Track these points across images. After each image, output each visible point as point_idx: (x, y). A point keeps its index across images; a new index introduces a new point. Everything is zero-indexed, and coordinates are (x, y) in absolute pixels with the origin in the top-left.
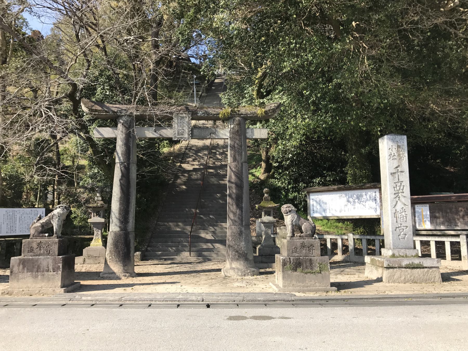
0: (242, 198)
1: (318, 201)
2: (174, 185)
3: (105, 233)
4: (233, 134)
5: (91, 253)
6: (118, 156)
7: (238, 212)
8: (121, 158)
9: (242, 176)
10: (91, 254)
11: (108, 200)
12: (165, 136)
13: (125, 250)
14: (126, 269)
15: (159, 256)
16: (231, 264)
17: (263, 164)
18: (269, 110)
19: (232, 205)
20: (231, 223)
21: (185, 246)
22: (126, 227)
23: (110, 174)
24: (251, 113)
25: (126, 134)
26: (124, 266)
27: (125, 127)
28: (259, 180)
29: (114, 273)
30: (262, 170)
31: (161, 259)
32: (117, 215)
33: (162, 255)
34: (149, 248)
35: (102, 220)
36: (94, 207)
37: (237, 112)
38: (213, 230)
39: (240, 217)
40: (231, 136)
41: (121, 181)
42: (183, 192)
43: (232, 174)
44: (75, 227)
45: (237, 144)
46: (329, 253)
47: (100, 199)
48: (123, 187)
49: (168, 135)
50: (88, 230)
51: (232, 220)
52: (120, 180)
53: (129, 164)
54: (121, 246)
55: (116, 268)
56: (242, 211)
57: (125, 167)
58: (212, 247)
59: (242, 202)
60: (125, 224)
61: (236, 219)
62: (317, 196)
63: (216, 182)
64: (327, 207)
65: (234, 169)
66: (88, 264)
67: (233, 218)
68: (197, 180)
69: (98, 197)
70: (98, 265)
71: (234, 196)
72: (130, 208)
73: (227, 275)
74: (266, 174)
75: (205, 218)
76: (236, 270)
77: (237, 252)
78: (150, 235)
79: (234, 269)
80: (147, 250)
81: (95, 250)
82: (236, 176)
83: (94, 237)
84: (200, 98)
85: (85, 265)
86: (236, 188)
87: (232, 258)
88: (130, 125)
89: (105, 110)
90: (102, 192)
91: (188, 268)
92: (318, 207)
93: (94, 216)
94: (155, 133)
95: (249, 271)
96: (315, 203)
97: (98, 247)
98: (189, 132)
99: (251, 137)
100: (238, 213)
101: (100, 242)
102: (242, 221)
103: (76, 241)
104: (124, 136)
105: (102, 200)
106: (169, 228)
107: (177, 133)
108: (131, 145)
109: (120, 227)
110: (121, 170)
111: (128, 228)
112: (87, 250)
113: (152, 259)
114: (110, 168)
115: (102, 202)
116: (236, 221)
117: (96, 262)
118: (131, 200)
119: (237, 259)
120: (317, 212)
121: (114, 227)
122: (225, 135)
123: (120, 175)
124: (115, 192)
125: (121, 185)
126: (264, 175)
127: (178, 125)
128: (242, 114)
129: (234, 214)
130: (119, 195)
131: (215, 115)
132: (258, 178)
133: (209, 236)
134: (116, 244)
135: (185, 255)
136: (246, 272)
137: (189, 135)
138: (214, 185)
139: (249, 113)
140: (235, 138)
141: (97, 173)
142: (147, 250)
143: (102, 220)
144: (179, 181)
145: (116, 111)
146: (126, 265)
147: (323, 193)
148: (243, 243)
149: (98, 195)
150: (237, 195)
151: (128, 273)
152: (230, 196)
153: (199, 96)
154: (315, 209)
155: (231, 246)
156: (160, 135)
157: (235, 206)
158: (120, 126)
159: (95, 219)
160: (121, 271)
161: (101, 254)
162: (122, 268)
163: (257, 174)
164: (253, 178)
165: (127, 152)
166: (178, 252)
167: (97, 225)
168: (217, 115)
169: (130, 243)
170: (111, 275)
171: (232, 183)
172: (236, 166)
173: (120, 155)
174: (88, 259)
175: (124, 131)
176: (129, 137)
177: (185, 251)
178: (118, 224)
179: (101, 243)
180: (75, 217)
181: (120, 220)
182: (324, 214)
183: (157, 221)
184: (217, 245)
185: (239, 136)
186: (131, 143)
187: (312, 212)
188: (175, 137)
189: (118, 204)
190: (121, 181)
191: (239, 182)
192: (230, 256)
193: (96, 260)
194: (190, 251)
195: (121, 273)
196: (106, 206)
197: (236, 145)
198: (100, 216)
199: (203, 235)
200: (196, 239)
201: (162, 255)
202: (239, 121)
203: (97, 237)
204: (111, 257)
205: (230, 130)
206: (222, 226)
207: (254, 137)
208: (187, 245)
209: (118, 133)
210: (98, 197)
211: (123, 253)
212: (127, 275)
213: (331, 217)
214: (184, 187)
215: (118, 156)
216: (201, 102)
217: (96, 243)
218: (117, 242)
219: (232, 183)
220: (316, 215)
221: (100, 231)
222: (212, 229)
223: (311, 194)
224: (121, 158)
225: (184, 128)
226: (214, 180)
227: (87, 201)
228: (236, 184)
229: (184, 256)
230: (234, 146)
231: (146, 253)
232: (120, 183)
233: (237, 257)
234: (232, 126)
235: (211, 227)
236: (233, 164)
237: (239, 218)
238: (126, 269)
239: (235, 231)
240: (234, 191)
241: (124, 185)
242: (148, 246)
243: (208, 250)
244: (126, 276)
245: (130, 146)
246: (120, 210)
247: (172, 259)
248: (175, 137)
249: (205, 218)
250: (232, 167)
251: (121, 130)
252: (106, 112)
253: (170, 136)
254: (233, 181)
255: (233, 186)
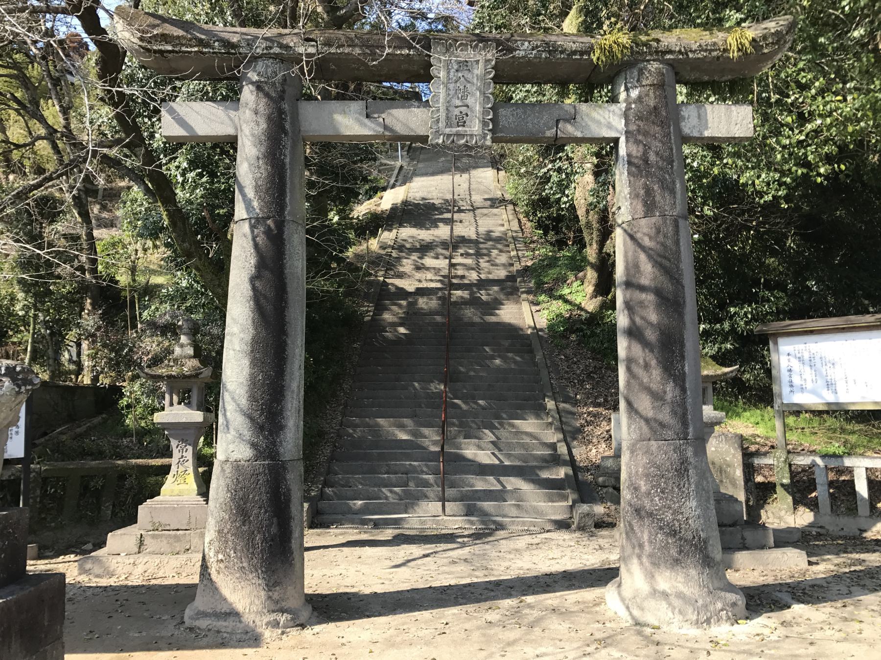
0: (682, 345)
1: (806, 356)
2: (377, 325)
3: (207, 451)
4: (640, 118)
5: (164, 519)
6: (244, 195)
7: (671, 391)
8: (255, 204)
9: (678, 267)
10: (163, 522)
11: (211, 357)
12: (401, 130)
13: (274, 530)
14: (276, 596)
15: (357, 512)
16: (651, 576)
17: (591, 275)
18: (765, 37)
19: (647, 366)
20: (645, 429)
21: (426, 484)
22: (274, 443)
23: (219, 285)
24: (701, 49)
25: (269, 119)
26: (271, 584)
27: (267, 95)
28: (583, 313)
29: (233, 614)
30: (590, 289)
31: (364, 522)
32: (244, 402)
33: (366, 510)
34: (329, 491)
35: (197, 416)
36: (170, 377)
37: (654, 44)
38: (493, 439)
39: (679, 410)
40: (633, 127)
41: (257, 284)
42: (399, 341)
43: (643, 257)
44: (127, 433)
45: (657, 154)
46: (863, 510)
47: (190, 351)
48: (263, 301)
49: (413, 126)
50: (156, 441)
51: (647, 421)
52: (253, 280)
53: (280, 225)
54: (259, 514)
55: (241, 593)
56: (683, 390)
57: (268, 232)
58: (499, 487)
59: (683, 357)
60: (271, 434)
61: (665, 415)
62: (801, 346)
63: (477, 319)
64: (836, 374)
65: (647, 242)
66: (153, 553)
67: (650, 414)
68: (432, 313)
69: (182, 346)
70: (183, 557)
71: (651, 335)
72: (287, 378)
73: (642, 619)
74: (600, 298)
75: (464, 406)
76: (677, 603)
77: (673, 533)
78: (328, 451)
79: (665, 595)
80: (322, 496)
81: (175, 509)
82: (657, 264)
83: (174, 461)
84: (408, 151)
85: (142, 559)
86: (658, 306)
87: (650, 556)
88: (283, 91)
89: (196, 38)
90: (194, 330)
91: (461, 568)
92: (808, 373)
93: (171, 404)
94: (366, 121)
95: (719, 605)
96: (795, 365)
97: (185, 498)
98: (485, 112)
99: (696, 134)
100: (669, 396)
101: (191, 485)
102: (685, 424)
103: (122, 475)
104: (264, 125)
105: (197, 354)
106: (376, 430)
107: (442, 115)
108: (287, 160)
109: (254, 445)
110: (256, 246)
111: (282, 450)
112: (152, 510)
113: (339, 523)
114: (219, 269)
115: (195, 362)
116: (662, 425)
117: (178, 547)
118: (289, 351)
119: (677, 562)
120: (802, 389)
121: (233, 446)
122: (610, 126)
123: (253, 261)
124: (233, 335)
125: (257, 298)
126: (594, 300)
127: (448, 89)
128: (671, 52)
129: (657, 397)
130: (248, 336)
131: (574, 52)
132: (580, 308)
133: (485, 457)
134: (241, 509)
135: (428, 514)
136: (712, 608)
137: (484, 124)
138: (473, 324)
139: (694, 47)
140: (646, 134)
141: (187, 288)
142: (322, 496)
143: (197, 416)
144: (387, 316)
145: (235, 39)
146: (276, 584)
147: (824, 336)
148: (693, 504)
149: (184, 339)
150: (662, 333)
151: (283, 611)
152: (633, 333)
153: (406, 148)
154: (796, 380)
155: (650, 515)
156: (386, 127)
157: (656, 373)
158: (248, 94)
159: (177, 413)
160: (258, 605)
161: (193, 520)
162: (263, 593)
163: (578, 299)
164: (568, 307)
165: (272, 182)
166: (410, 501)
167: (183, 430)
168: (582, 53)
169: (288, 501)
170: (222, 623)
171: (642, 288)
172: (658, 231)
173: (250, 193)
174: (154, 537)
175: (262, 107)
176: (279, 132)
177: (426, 497)
178: (247, 434)
179: (195, 487)
180: (129, 406)
181: (251, 418)
182: (831, 399)
183: (344, 415)
184: (513, 483)
185: (662, 124)
186: (287, 152)
187: (786, 390)
188: (437, 133)
189: (246, 362)
190: (257, 284)
191: (668, 286)
192: (647, 548)
193: (177, 539)
194: (443, 500)
195: (261, 613)
196: (207, 372)
197: (652, 157)
198: (189, 405)
199: (471, 451)
200: (453, 466)
201: (366, 510)
202: (660, 73)
203: (181, 469)
204: (225, 553)
205: (628, 109)
206: (513, 426)
207: (706, 134)
208: (432, 481)
209: (242, 121)
210: (183, 347)
211: (264, 540)
212: (283, 618)
213: (854, 403)
214: (402, 330)
215: (244, 195)
216: (412, 159)
217: (179, 486)
218: (245, 499)
219: (642, 288)
220: (799, 399)
221: (190, 448)
222: (489, 436)
223: (781, 341)
224: (255, 204)
225: (470, 101)
226: (469, 313)
227: (156, 361)
228: (658, 292)
229: (426, 511)
230: (646, 161)
231: (323, 505)
232: (254, 288)
233: (674, 552)
234: (634, 93)
235: (487, 431)
236: (645, 226)
237: (674, 413)
238: (276, 596)
239: (660, 458)
240: (653, 317)
241: (265, 297)
242: (326, 484)
243: (489, 495)
244: (276, 624)
245: (284, 164)
246: (253, 383)
247: (396, 523)
248: (437, 133)
249: (464, 406)
250: (639, 236)
251: (252, 105)
252: (201, 43)
253: (421, 132)
254: (645, 281)
255: (649, 298)
